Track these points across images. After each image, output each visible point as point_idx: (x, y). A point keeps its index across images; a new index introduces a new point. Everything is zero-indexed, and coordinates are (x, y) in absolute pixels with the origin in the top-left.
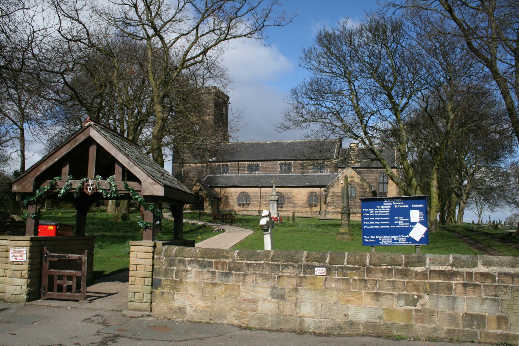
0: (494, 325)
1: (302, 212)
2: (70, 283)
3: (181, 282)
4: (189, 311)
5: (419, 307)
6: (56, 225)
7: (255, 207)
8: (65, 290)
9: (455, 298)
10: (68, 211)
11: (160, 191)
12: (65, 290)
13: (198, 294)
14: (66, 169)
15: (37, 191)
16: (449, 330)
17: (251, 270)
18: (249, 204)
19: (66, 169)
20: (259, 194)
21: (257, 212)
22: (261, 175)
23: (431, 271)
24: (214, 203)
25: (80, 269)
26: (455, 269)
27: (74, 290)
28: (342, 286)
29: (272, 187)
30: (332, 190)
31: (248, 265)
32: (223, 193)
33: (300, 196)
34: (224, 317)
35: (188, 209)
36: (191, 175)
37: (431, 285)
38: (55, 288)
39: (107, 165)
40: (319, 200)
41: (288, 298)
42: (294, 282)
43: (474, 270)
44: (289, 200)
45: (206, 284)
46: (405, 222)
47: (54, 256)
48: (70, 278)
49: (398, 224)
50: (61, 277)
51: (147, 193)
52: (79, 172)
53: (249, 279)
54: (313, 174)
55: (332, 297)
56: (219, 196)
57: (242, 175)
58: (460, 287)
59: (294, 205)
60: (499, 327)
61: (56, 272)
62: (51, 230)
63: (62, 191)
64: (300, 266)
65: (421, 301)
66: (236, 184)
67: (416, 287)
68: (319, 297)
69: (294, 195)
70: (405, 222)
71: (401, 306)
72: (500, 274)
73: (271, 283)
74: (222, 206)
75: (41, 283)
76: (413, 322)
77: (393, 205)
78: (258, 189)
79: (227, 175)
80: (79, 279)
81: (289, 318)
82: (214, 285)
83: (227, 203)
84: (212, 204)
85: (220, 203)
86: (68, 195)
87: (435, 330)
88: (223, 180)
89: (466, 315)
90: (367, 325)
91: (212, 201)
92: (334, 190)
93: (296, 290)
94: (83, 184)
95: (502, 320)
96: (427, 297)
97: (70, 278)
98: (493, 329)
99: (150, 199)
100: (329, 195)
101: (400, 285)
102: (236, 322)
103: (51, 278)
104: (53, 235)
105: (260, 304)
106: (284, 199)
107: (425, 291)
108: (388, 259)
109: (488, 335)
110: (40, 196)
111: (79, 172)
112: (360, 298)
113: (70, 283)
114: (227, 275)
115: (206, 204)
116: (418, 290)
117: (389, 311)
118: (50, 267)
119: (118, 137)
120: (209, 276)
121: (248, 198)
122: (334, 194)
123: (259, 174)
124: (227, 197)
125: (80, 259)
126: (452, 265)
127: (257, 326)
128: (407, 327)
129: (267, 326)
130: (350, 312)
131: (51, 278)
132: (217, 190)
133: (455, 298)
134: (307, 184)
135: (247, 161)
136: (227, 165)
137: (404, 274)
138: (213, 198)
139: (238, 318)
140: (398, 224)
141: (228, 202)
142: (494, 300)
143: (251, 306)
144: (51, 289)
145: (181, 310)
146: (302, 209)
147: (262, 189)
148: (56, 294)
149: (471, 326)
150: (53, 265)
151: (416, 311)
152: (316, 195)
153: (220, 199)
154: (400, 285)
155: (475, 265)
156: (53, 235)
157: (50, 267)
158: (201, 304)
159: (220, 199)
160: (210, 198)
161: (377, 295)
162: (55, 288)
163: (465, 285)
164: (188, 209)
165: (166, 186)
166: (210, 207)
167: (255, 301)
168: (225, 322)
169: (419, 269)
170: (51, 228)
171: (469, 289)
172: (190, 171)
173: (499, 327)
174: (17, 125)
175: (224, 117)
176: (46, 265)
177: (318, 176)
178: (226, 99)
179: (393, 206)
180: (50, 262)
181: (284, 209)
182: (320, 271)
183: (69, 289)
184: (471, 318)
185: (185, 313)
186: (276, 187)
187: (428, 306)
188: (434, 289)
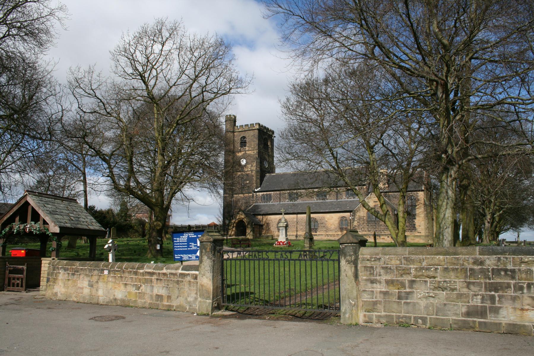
0: (166, 300)
1: (334, 236)
2: (18, 282)
3: (57, 279)
4: (59, 294)
5: (140, 291)
6: (26, 250)
7: (293, 231)
8: (16, 286)
9: (153, 286)
10: (135, 239)
11: (57, 230)
12: (16, 286)
13: (62, 285)
14: (17, 219)
15: (3, 231)
16: (150, 303)
17: (82, 272)
18: (316, 229)
19: (17, 219)
20: (296, 220)
21: (295, 236)
22: (300, 202)
23: (146, 272)
24: (256, 229)
25: (23, 274)
26: (154, 271)
27: (20, 286)
28: (114, 280)
29: (281, 214)
30: (358, 214)
31: (81, 269)
32: (264, 220)
33: (331, 221)
34: (71, 297)
35: (233, 235)
36: (239, 204)
37: (145, 279)
38: (11, 285)
39: (36, 217)
40: (349, 224)
41: (94, 286)
42: (96, 277)
43: (161, 272)
44: (323, 225)
45: (66, 280)
46: (195, 246)
47: (11, 267)
48: (18, 279)
49: (191, 247)
50: (14, 279)
51: (52, 232)
52: (24, 221)
53: (82, 276)
54: (346, 200)
55: (110, 285)
56: (261, 223)
57: (284, 203)
58: (155, 280)
59: (327, 230)
60: (168, 302)
61: (12, 275)
62: (23, 253)
63: (15, 231)
64: (99, 270)
65: (141, 288)
66: (276, 212)
67: (140, 280)
68: (105, 285)
69: (326, 220)
70: (195, 246)
71: (133, 290)
72: (170, 273)
73: (89, 279)
74: (264, 232)
75: (4, 282)
76: (138, 299)
77: (189, 236)
78: (295, 216)
79: (271, 203)
80: (22, 279)
81: (94, 297)
82: (69, 280)
83: (268, 229)
84: (253, 231)
85: (263, 229)
86: (18, 232)
87: (145, 302)
88: (266, 208)
89: (157, 295)
90: (123, 300)
91: (253, 228)
92: (360, 214)
93: (97, 282)
94: (25, 226)
95: (169, 297)
96: (143, 286)
97: (18, 279)
98: (165, 303)
99: (54, 234)
100: (356, 219)
101: (134, 280)
102: (75, 299)
103: (9, 279)
104: (24, 255)
105: (84, 290)
106: (318, 224)
107: (143, 283)
108: (131, 266)
109: (163, 305)
110: (5, 234)
111: (24, 221)
112: (120, 286)
113: (18, 282)
114: (73, 274)
115: (248, 231)
116: (140, 282)
117: (129, 293)
118: (9, 273)
119: (52, 198)
120: (67, 275)
121: (316, 223)
122: (360, 218)
123: (299, 201)
124: (268, 224)
125: (23, 269)
126: (154, 269)
127: (82, 301)
128: (135, 301)
129: (86, 302)
130: (116, 294)
131: (9, 279)
132: (260, 217)
133: (153, 286)
134: (338, 210)
135: (287, 190)
136: (270, 194)
137: (136, 273)
138: (254, 224)
139: (76, 297)
140: (191, 247)
141: (269, 229)
142: (167, 287)
143: (81, 291)
144: (9, 286)
145: (56, 294)
146: (334, 233)
147: (299, 216)
148: (11, 288)
149: (157, 301)
150: (11, 272)
151: (139, 293)
152: (346, 220)
153: (262, 226)
154: (134, 280)
155: (162, 269)
156: (24, 255)
157: (9, 273)
158: (63, 290)
159: (262, 226)
160: (252, 225)
161: (126, 284)
162: (11, 285)
163: (157, 279)
164: (233, 235)
165: (60, 227)
166: (252, 233)
167: (82, 288)
168: (71, 299)
169: (141, 271)
170: (23, 251)
171: (159, 281)
172: (239, 200)
173: (168, 302)
174: (80, 170)
175: (270, 151)
176: (7, 272)
177: (351, 201)
178: (271, 133)
179: (189, 236)
180: (9, 270)
181: (318, 233)
182: (106, 272)
183: (18, 286)
184: (159, 297)
185: (57, 295)
186: (285, 214)
187: (143, 291)
188: (146, 281)
